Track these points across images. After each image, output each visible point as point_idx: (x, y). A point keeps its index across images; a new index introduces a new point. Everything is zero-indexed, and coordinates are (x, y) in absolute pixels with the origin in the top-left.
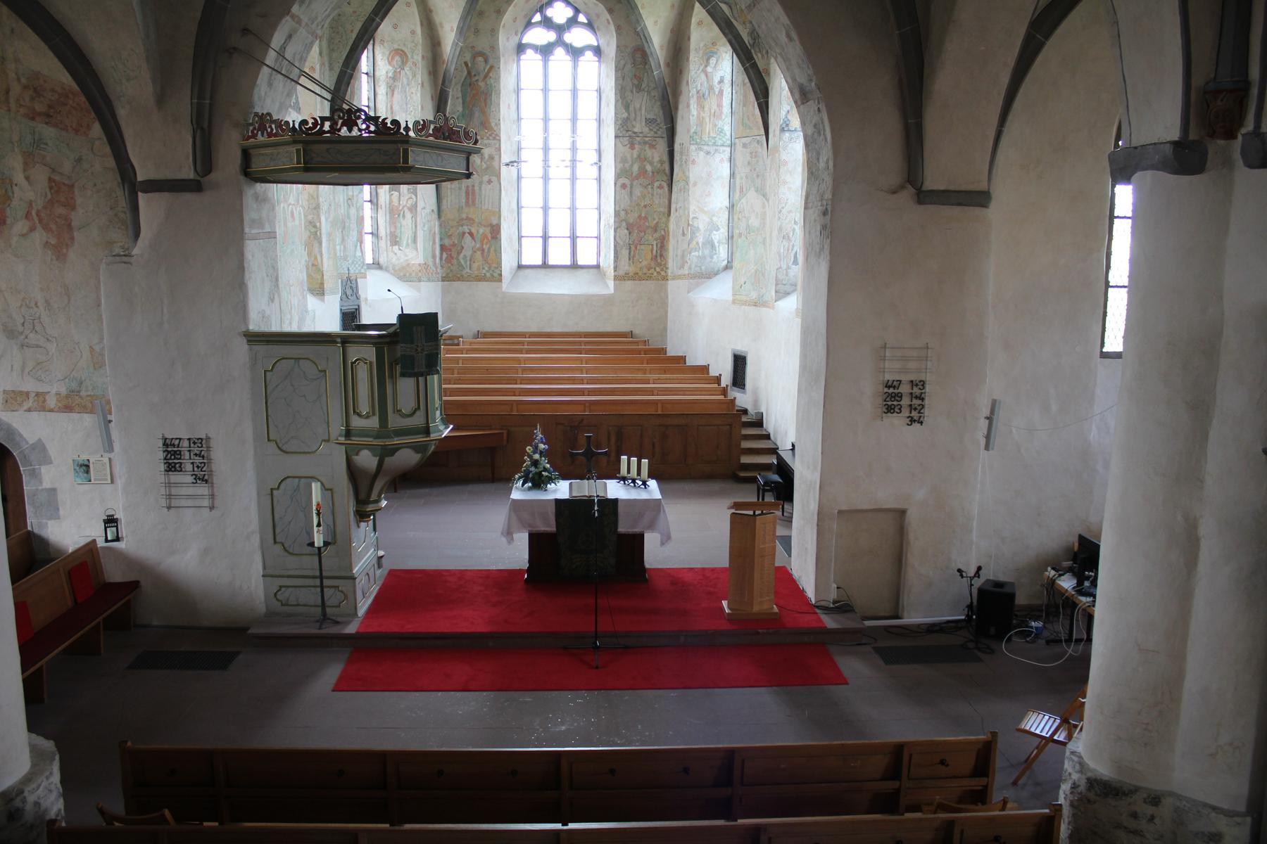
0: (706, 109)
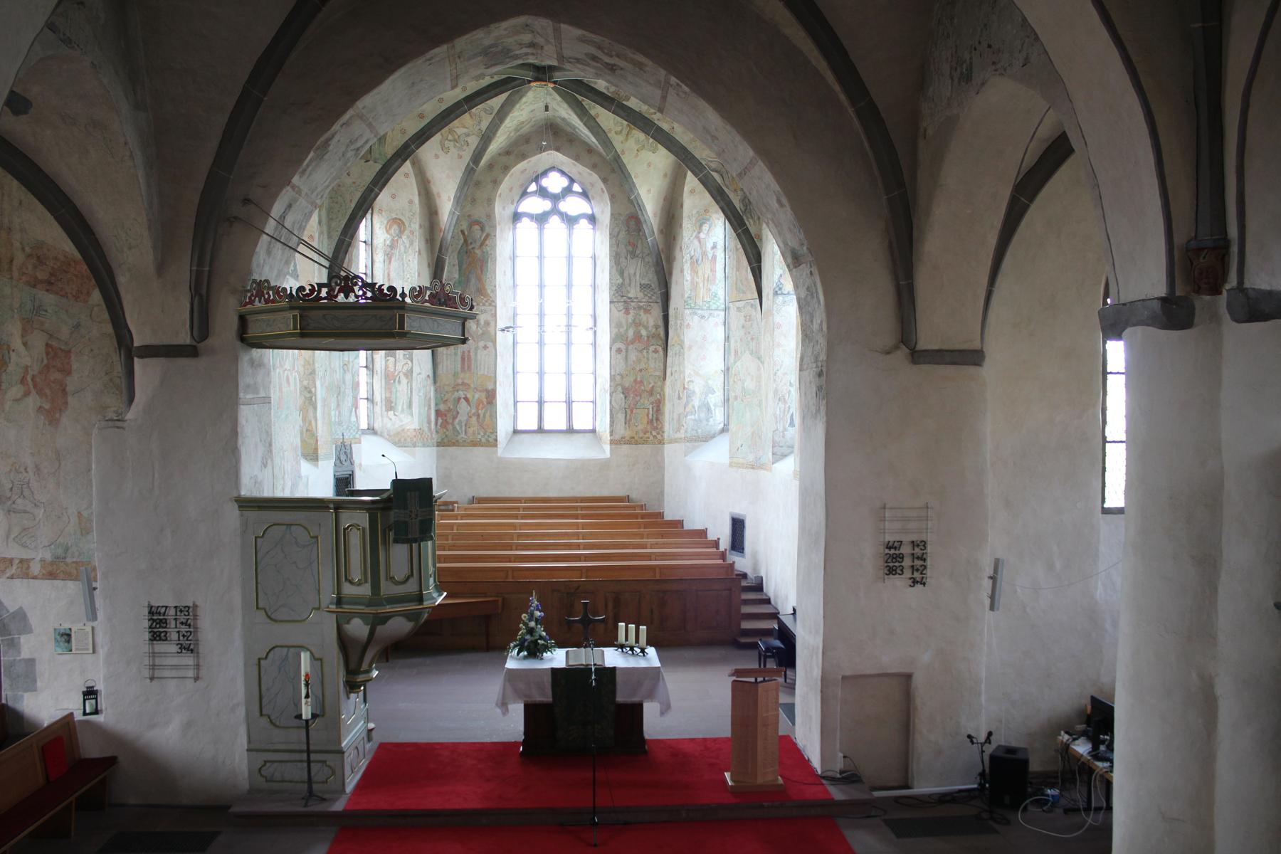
0: (700, 273)
